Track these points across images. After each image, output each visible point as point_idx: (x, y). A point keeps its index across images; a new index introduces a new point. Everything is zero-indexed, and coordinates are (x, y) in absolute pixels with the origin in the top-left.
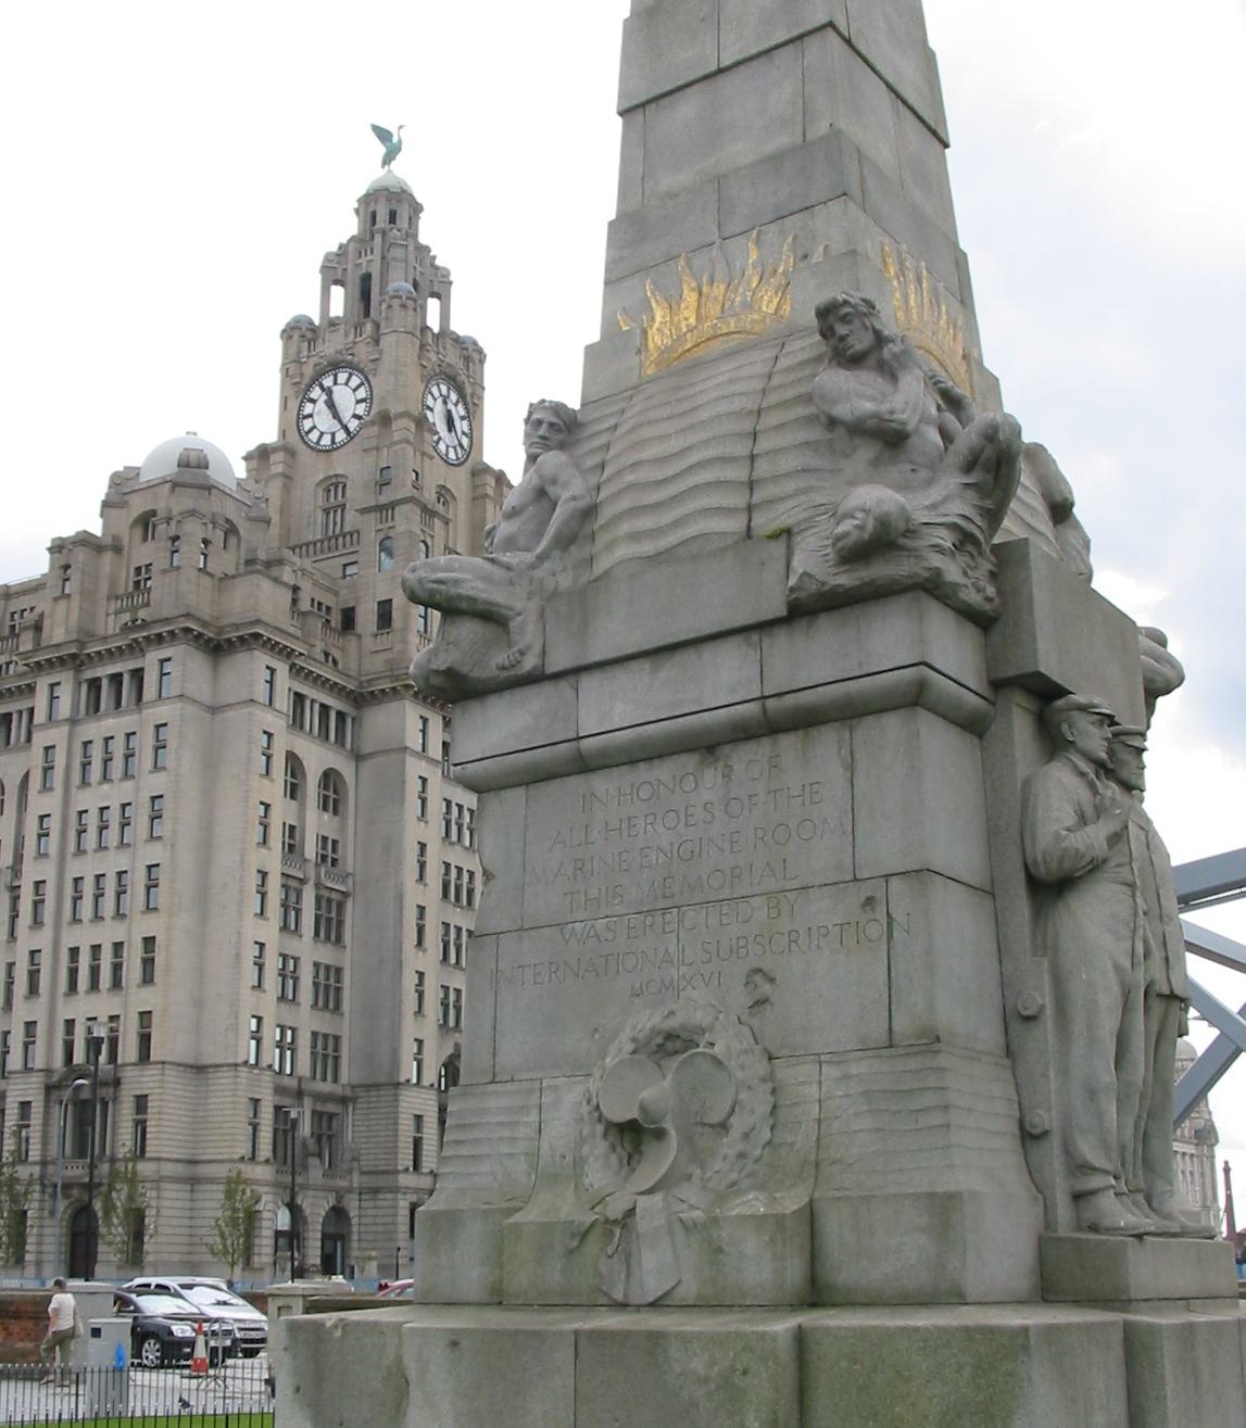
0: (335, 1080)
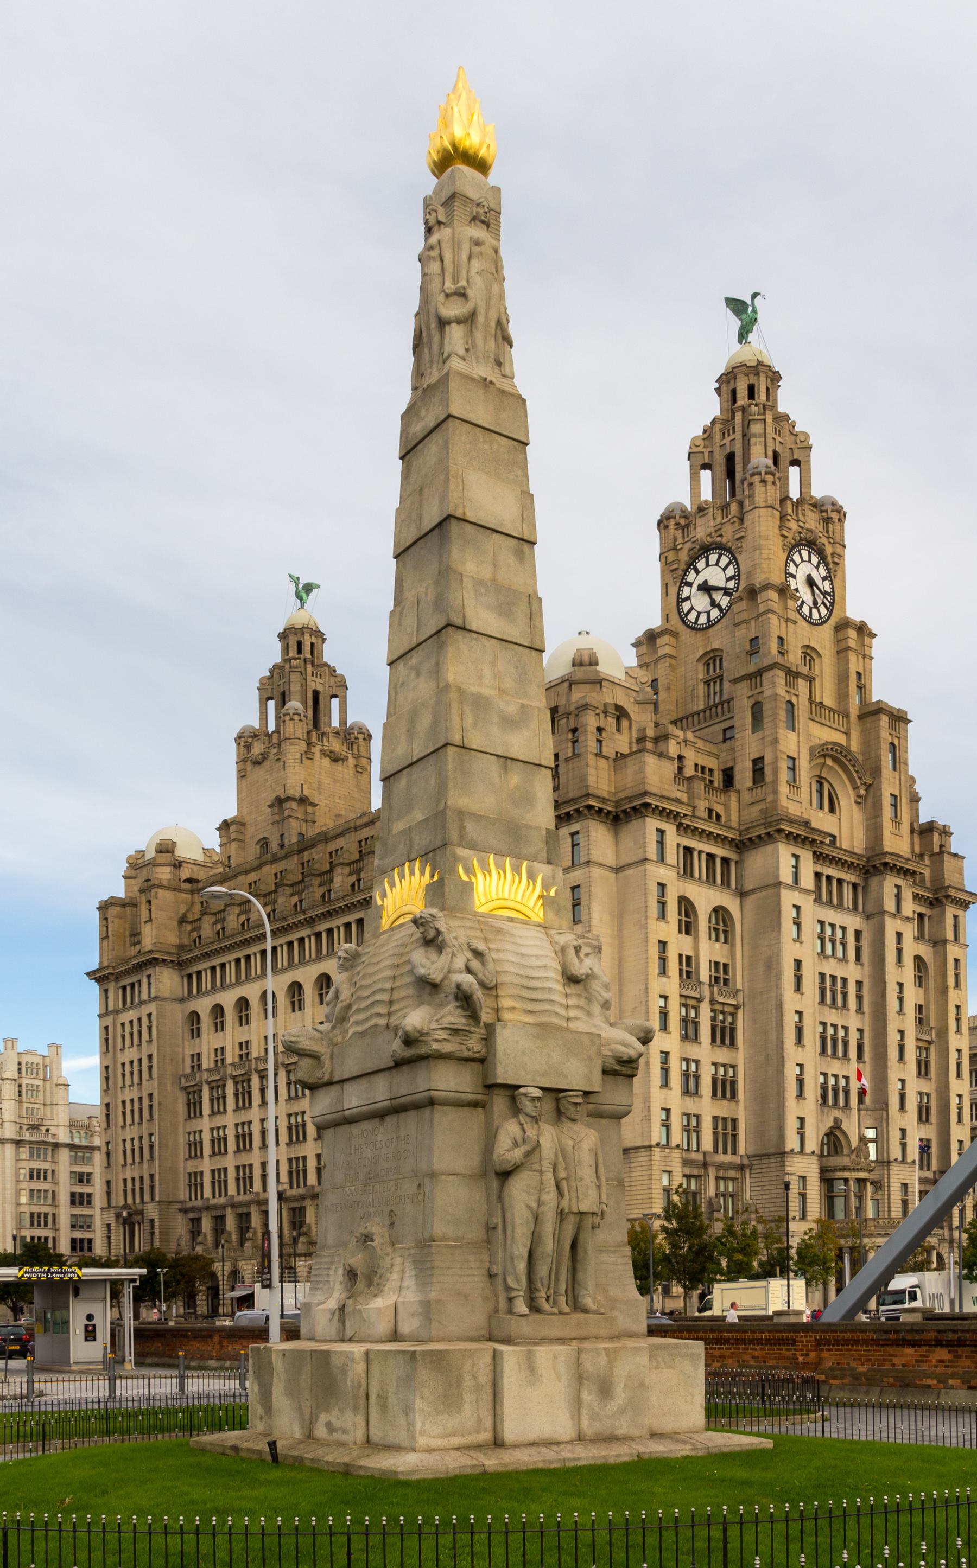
0: (734, 1152)
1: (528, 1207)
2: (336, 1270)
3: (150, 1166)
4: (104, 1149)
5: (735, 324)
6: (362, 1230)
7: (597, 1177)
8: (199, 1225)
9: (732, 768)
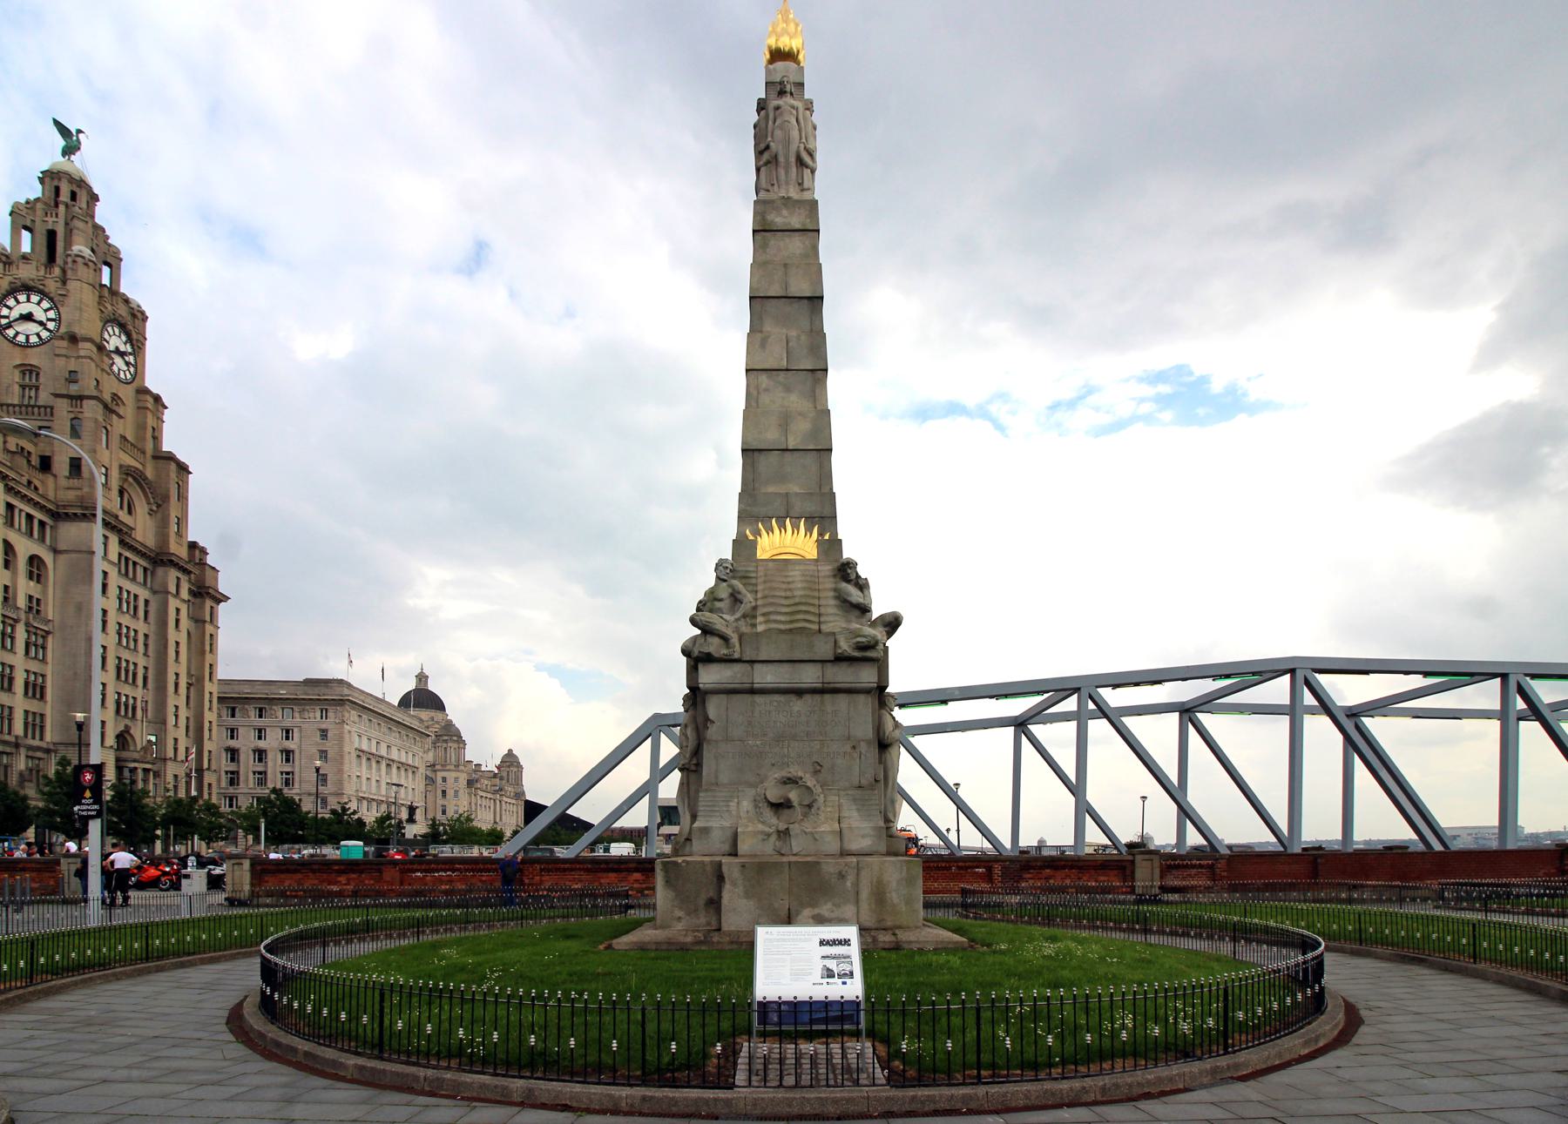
0: (42, 739)
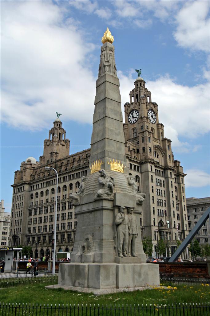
1: (123, 232)
2: (79, 246)
3: (20, 226)
4: (11, 222)
5: (137, 74)
6: (86, 237)
7: (136, 226)
8: (30, 239)
9: (139, 149)
